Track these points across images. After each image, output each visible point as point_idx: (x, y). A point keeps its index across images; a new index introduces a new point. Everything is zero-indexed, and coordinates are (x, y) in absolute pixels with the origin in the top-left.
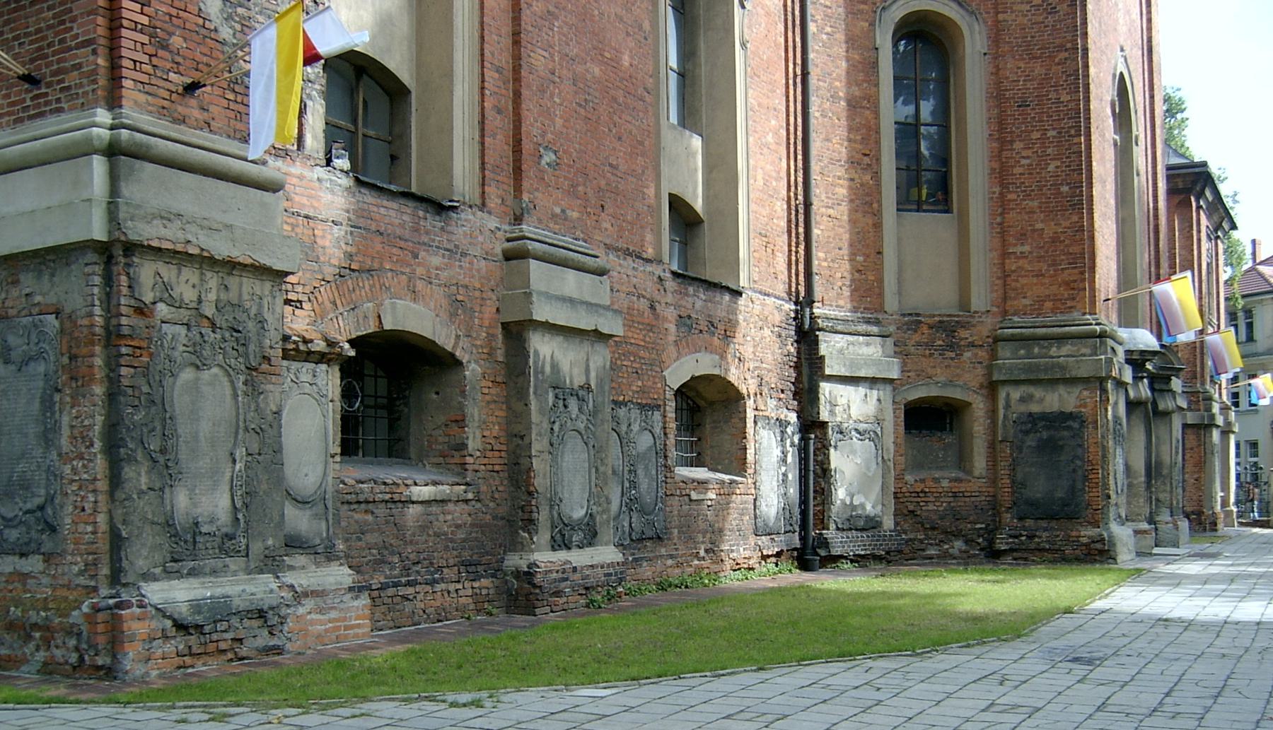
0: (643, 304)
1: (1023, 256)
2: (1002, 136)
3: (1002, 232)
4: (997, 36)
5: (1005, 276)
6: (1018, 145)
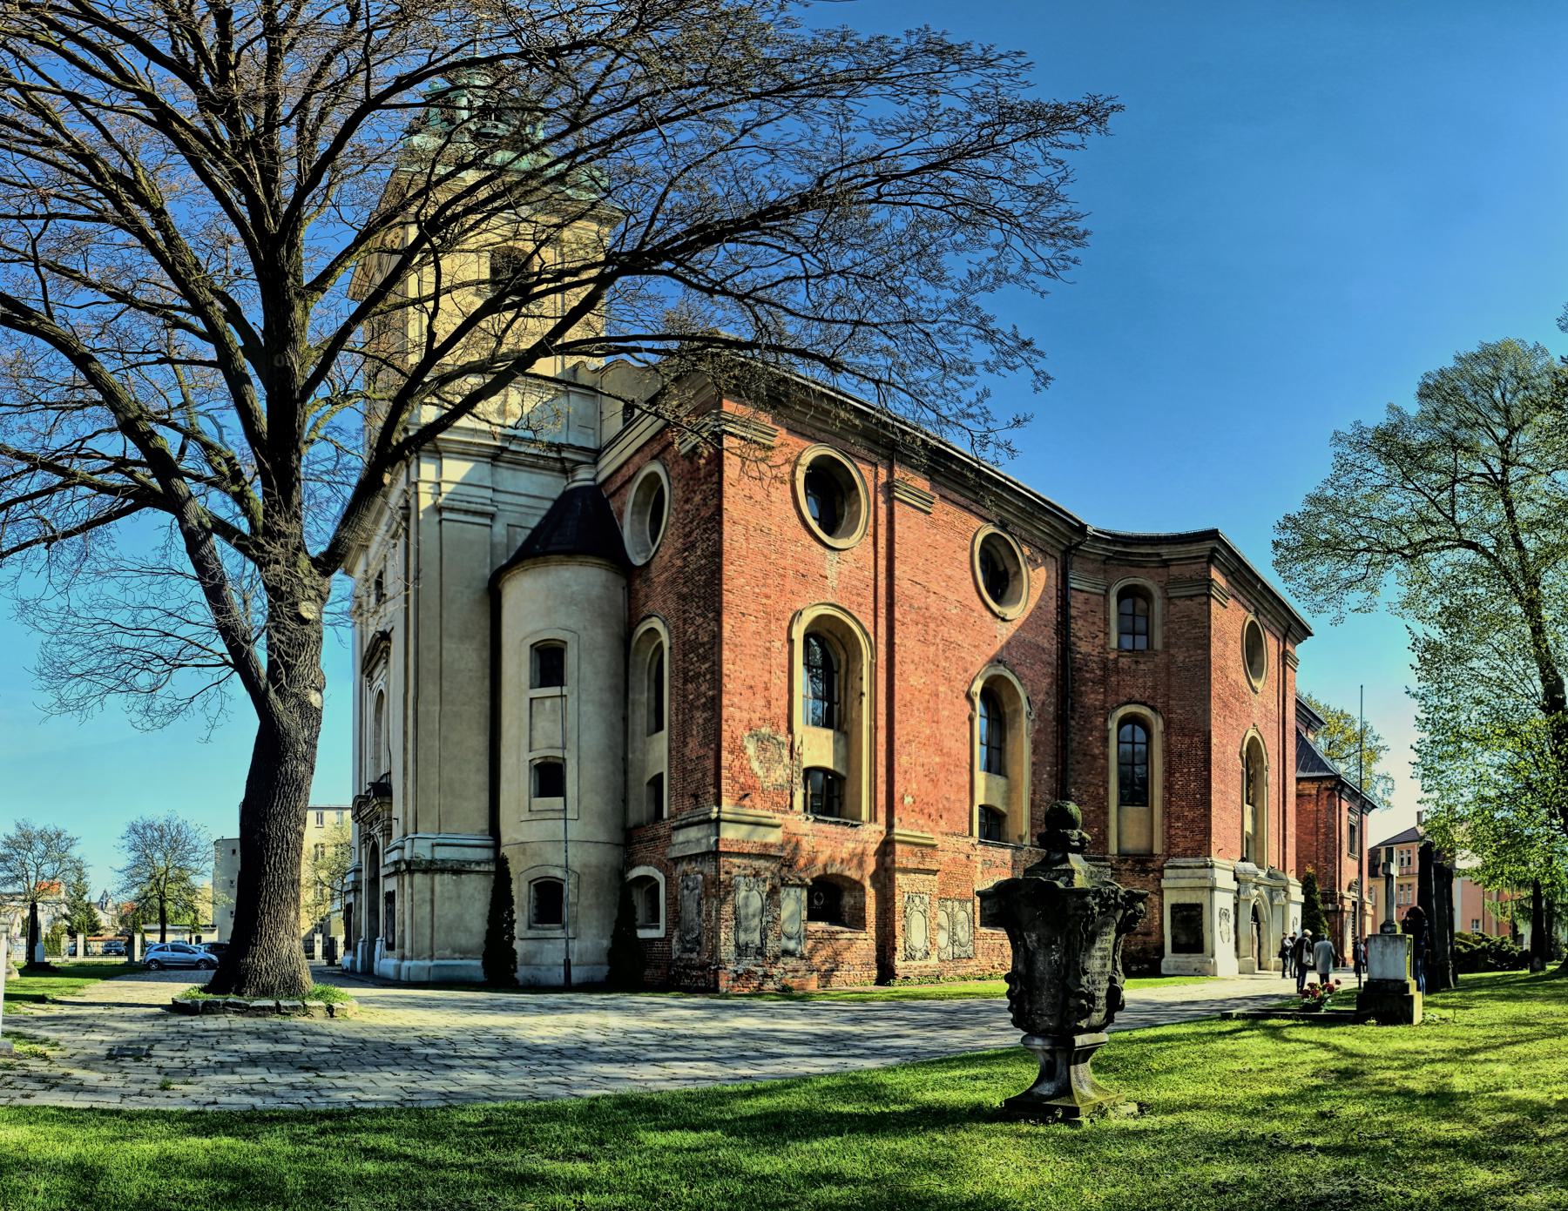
0: (963, 857)
1: (1178, 828)
2: (1169, 771)
3: (1167, 815)
4: (1168, 724)
5: (1170, 837)
6: (1177, 775)
